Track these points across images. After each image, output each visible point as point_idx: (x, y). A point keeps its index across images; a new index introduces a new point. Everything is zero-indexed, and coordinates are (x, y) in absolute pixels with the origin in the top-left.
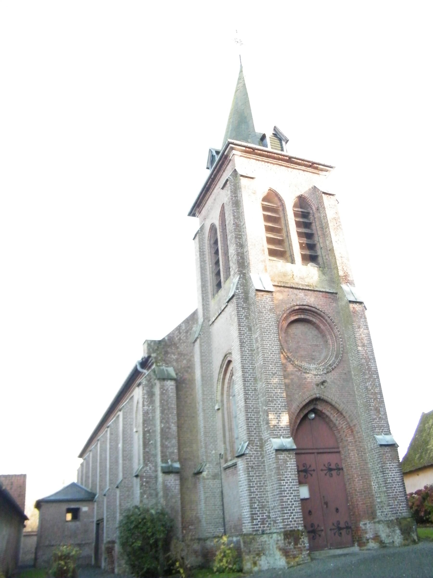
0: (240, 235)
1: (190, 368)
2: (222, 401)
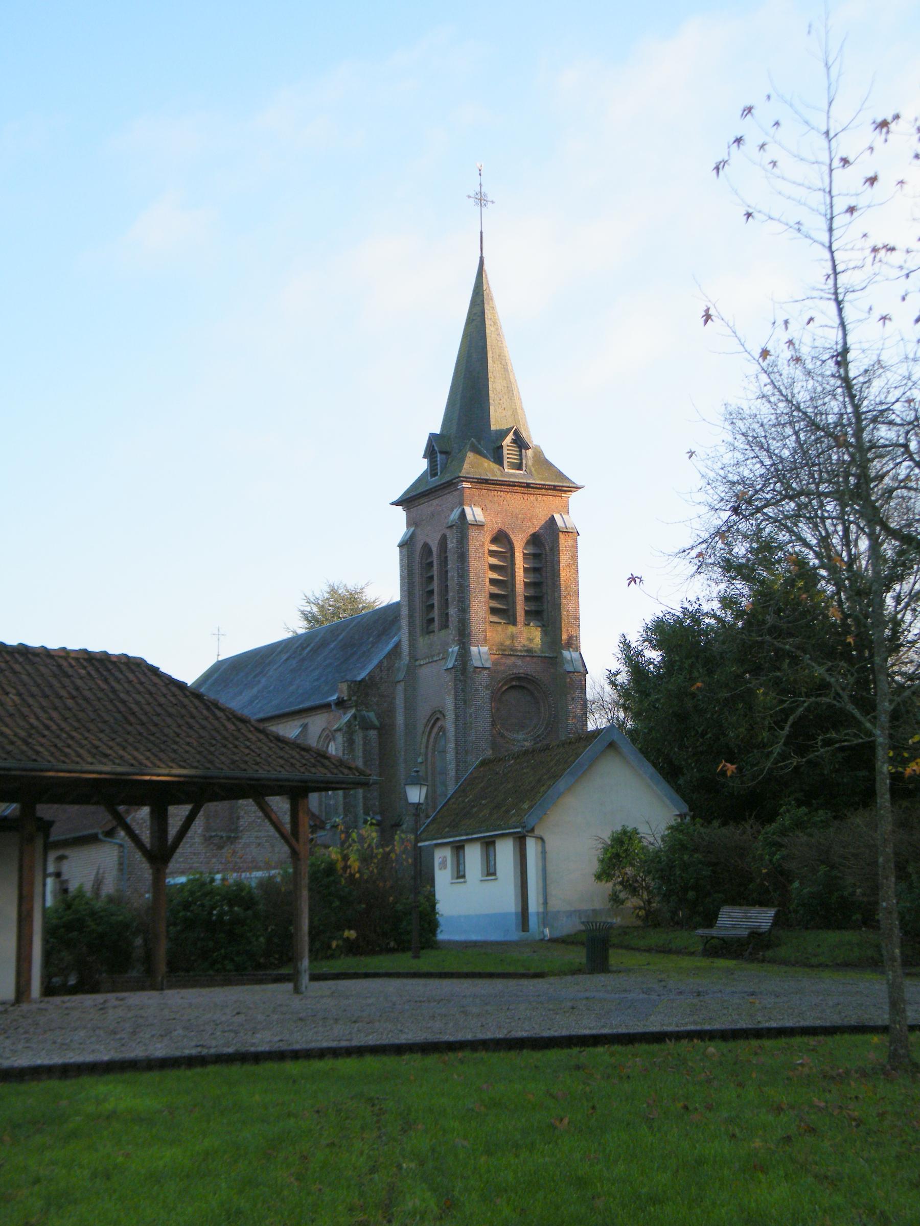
0: (463, 597)
1: (390, 712)
2: (426, 754)
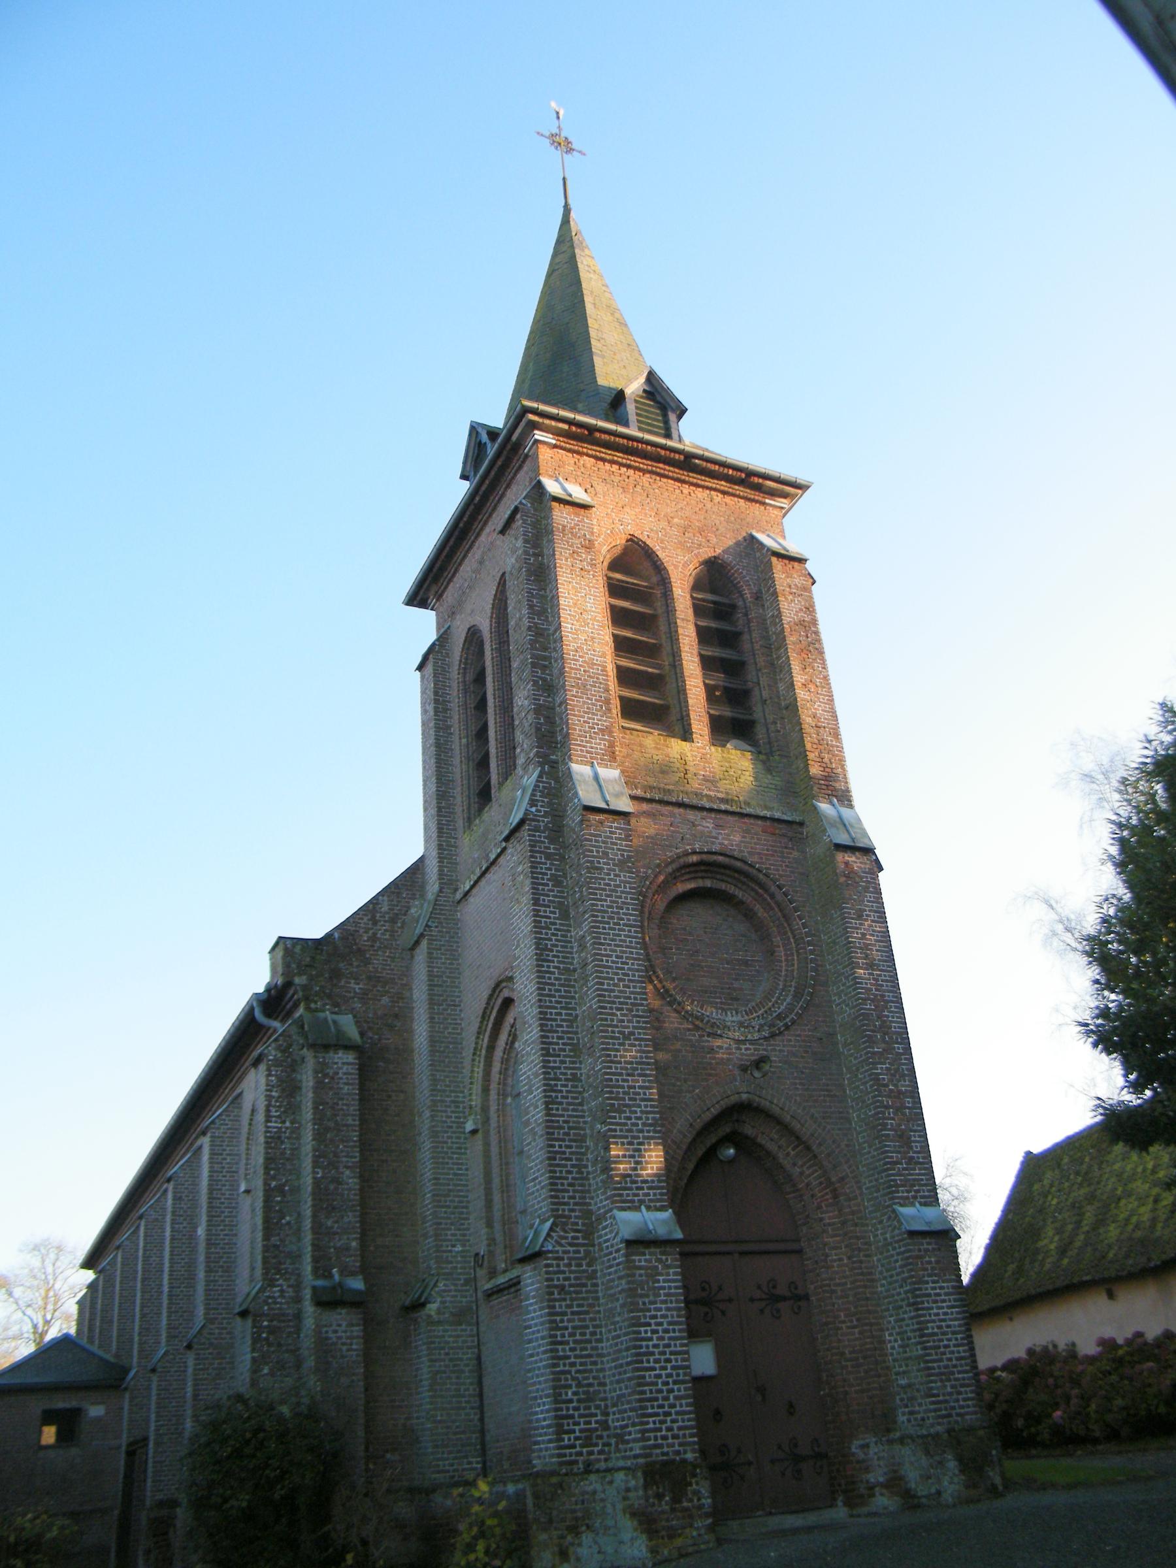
1: (399, 1016)
2: (485, 1109)
